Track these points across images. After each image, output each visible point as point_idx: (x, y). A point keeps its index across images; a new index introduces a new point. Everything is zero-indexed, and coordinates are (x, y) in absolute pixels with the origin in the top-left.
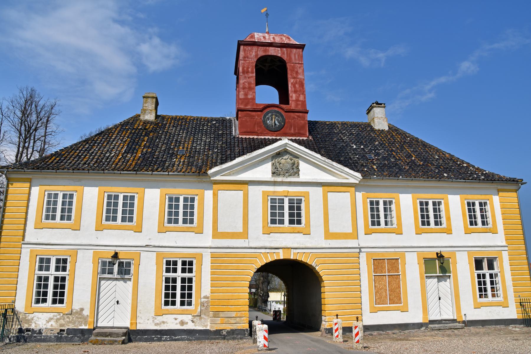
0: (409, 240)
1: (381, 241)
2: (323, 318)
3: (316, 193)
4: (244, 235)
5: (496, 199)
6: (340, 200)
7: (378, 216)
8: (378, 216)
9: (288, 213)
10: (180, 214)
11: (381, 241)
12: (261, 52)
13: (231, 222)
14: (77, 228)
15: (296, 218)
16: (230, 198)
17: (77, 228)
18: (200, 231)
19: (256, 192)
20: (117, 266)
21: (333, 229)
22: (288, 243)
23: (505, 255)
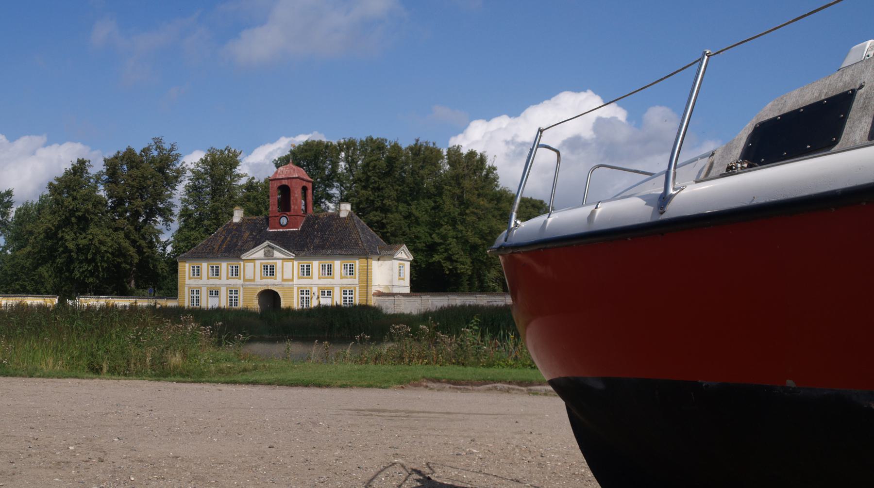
2: (357, 301)
3: (279, 263)
4: (292, 280)
5: (357, 262)
6: (288, 265)
8: (307, 272)
9: (270, 271)
12: (278, 184)
13: (249, 274)
14: (220, 279)
15: (272, 273)
16: (250, 265)
17: (220, 279)
18: (240, 279)
19: (258, 263)
20: (214, 293)
21: (247, 277)
22: (269, 283)
23: (357, 289)
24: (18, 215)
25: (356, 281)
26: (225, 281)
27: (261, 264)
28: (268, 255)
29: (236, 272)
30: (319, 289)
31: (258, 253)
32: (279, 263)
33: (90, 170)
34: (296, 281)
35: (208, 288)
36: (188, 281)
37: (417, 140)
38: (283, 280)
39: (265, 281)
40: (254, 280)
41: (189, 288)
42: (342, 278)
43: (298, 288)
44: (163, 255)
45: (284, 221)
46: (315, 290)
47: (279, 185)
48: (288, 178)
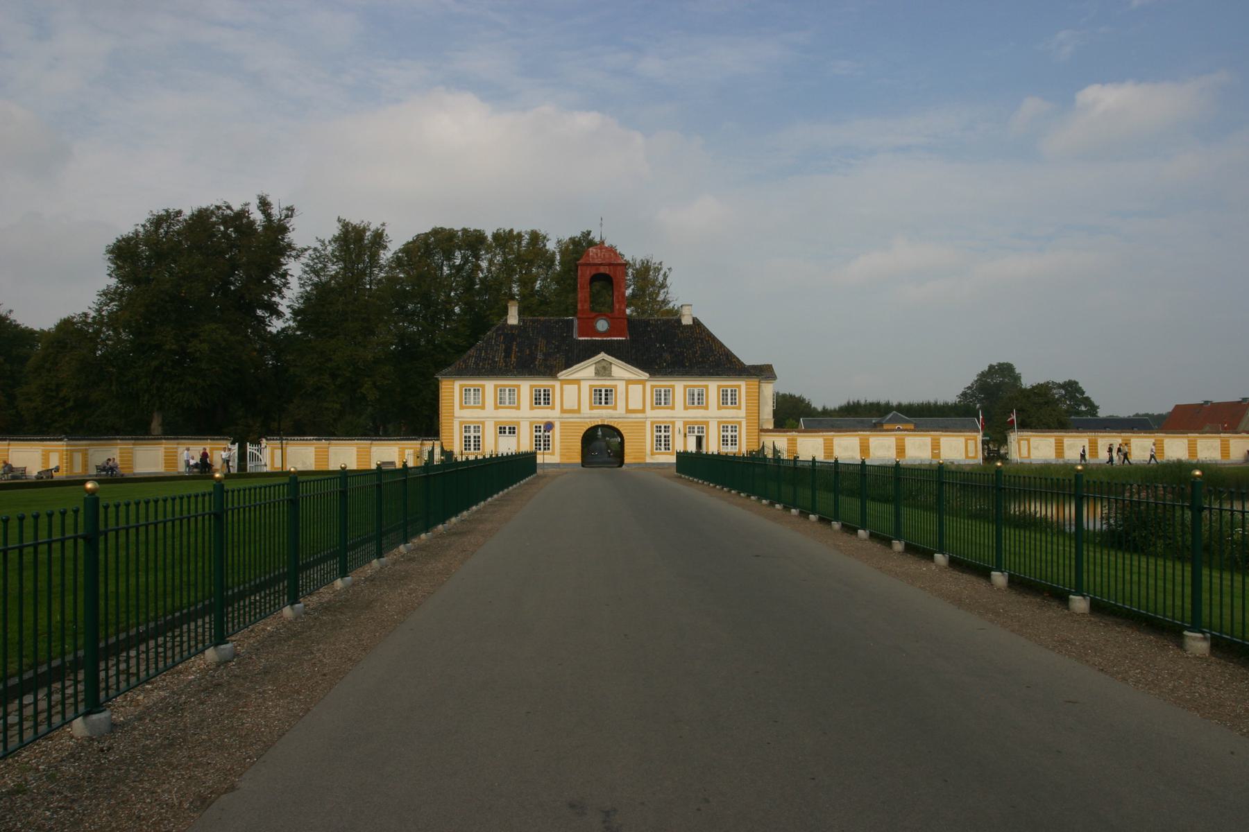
0: (679, 413)
1: (662, 414)
4: (643, 411)
6: (636, 390)
7: (697, 400)
8: (662, 400)
9: (603, 397)
10: (543, 398)
11: (662, 414)
13: (570, 403)
16: (571, 390)
18: (553, 408)
22: (602, 415)
23: (744, 424)
24: (309, 312)
25: (742, 413)
26: (526, 414)
27: (591, 387)
28: (603, 371)
29: (543, 398)
30: (685, 423)
31: (585, 371)
32: (621, 386)
33: (113, 286)
34: (650, 413)
35: (496, 423)
36: (458, 412)
37: (11, 311)
38: (628, 411)
39: (596, 412)
40: (578, 411)
41: (462, 423)
42: (686, 408)
43: (652, 423)
44: (131, 341)
45: (602, 325)
46: (679, 425)
47: (593, 272)
48: (610, 265)
